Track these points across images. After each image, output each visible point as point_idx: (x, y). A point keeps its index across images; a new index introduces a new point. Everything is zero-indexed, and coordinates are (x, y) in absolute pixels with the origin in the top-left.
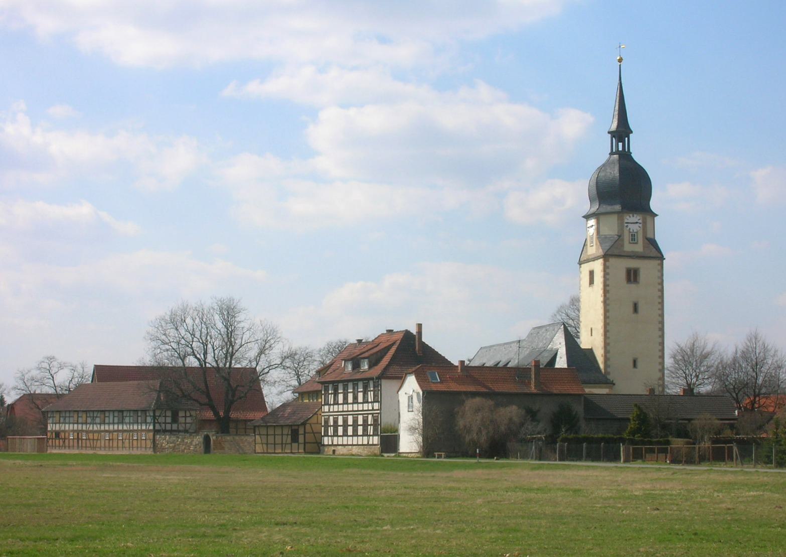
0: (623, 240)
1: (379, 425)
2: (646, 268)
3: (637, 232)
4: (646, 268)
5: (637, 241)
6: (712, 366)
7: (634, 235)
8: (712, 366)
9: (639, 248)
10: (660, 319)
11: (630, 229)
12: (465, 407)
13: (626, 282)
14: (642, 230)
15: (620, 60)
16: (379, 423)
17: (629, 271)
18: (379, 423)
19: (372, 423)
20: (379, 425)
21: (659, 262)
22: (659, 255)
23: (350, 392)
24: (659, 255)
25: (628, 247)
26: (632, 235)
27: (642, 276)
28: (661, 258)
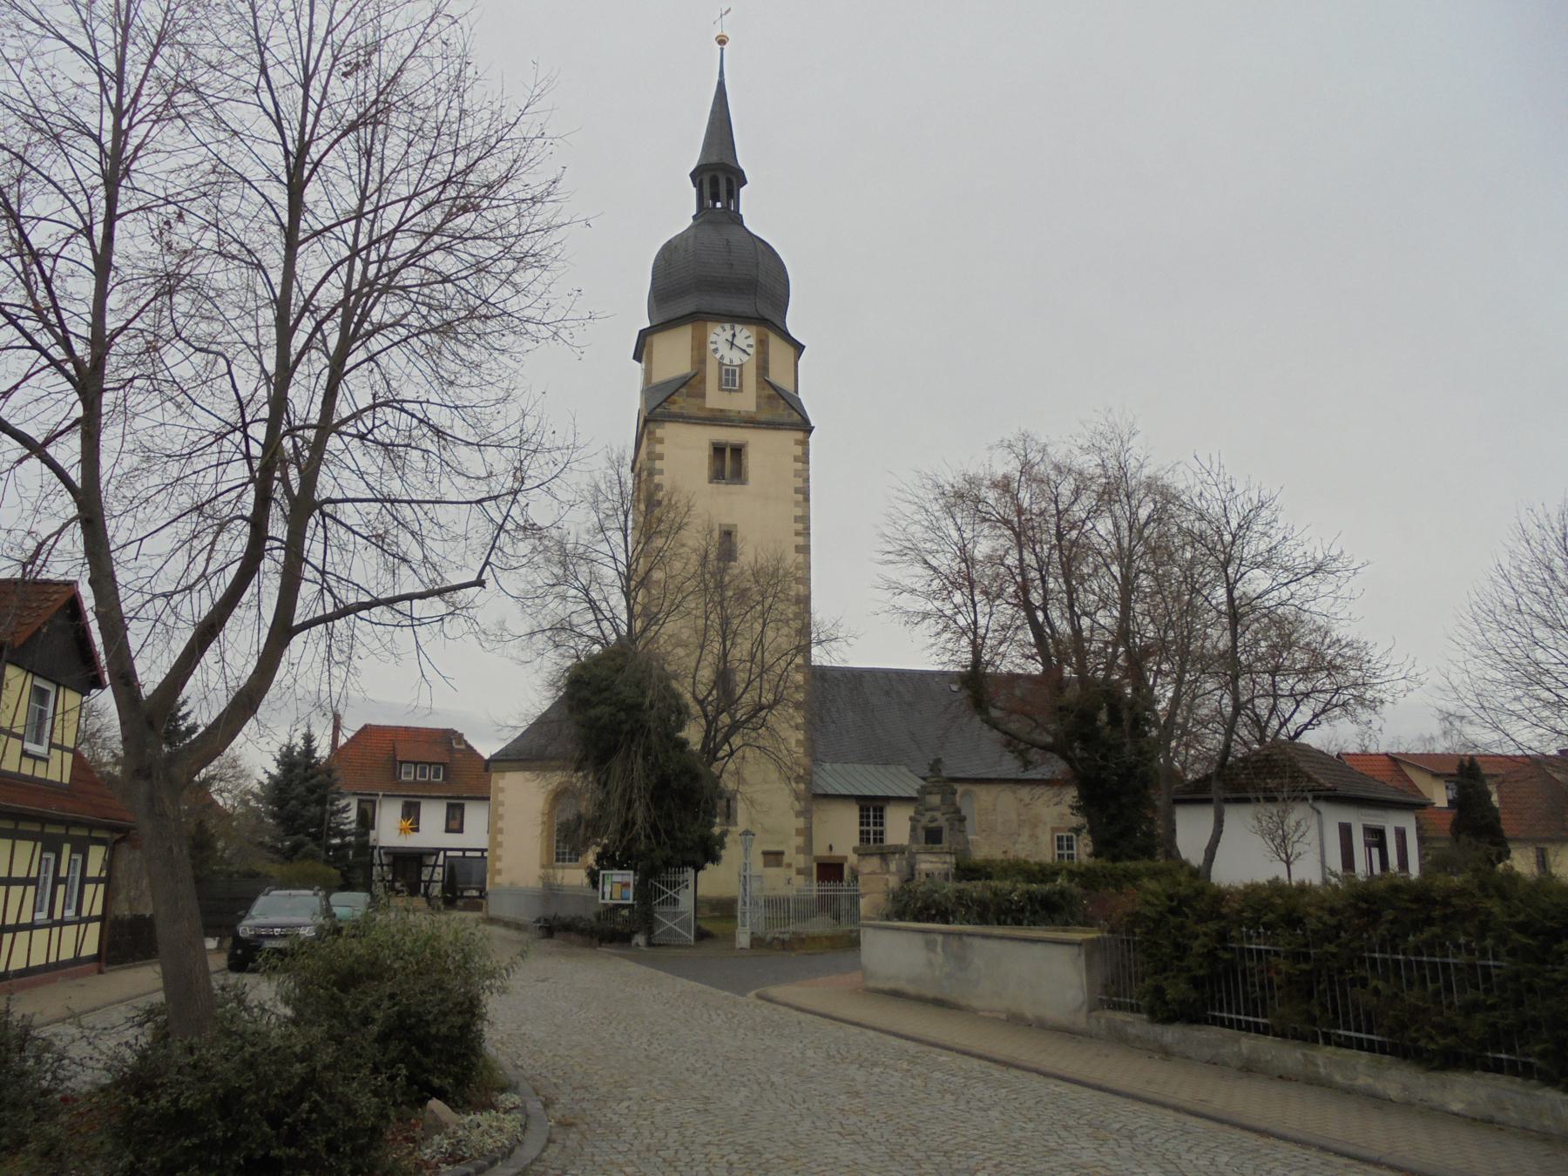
0: (703, 381)
1: (464, 856)
2: (765, 449)
3: (741, 366)
4: (765, 449)
5: (741, 385)
6: (355, 1117)
7: (734, 371)
8: (355, 1117)
9: (746, 401)
10: (799, 483)
11: (722, 357)
12: (1152, 822)
13: (707, 480)
14: (754, 361)
15: (722, 41)
16: (460, 854)
17: (718, 450)
18: (460, 854)
19: (103, 875)
20: (464, 856)
21: (800, 435)
22: (796, 418)
23: (1542, 862)
24: (796, 418)
25: (715, 399)
26: (727, 371)
27: (754, 461)
28: (807, 428)
